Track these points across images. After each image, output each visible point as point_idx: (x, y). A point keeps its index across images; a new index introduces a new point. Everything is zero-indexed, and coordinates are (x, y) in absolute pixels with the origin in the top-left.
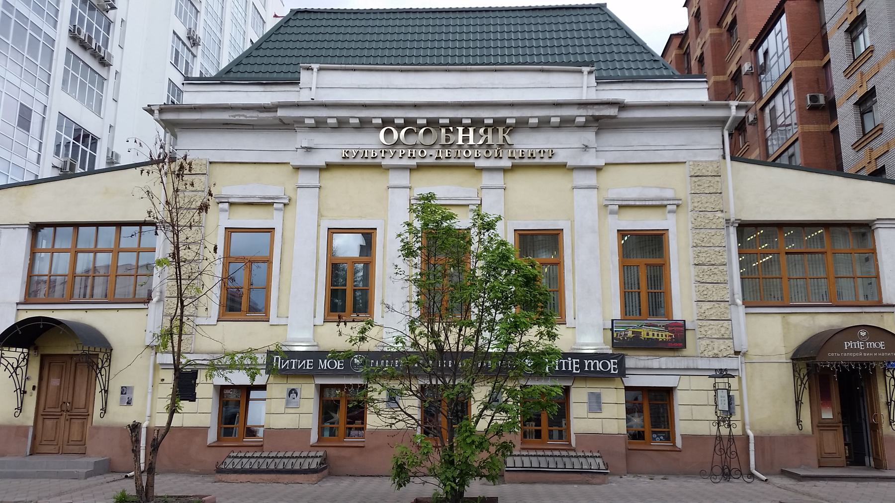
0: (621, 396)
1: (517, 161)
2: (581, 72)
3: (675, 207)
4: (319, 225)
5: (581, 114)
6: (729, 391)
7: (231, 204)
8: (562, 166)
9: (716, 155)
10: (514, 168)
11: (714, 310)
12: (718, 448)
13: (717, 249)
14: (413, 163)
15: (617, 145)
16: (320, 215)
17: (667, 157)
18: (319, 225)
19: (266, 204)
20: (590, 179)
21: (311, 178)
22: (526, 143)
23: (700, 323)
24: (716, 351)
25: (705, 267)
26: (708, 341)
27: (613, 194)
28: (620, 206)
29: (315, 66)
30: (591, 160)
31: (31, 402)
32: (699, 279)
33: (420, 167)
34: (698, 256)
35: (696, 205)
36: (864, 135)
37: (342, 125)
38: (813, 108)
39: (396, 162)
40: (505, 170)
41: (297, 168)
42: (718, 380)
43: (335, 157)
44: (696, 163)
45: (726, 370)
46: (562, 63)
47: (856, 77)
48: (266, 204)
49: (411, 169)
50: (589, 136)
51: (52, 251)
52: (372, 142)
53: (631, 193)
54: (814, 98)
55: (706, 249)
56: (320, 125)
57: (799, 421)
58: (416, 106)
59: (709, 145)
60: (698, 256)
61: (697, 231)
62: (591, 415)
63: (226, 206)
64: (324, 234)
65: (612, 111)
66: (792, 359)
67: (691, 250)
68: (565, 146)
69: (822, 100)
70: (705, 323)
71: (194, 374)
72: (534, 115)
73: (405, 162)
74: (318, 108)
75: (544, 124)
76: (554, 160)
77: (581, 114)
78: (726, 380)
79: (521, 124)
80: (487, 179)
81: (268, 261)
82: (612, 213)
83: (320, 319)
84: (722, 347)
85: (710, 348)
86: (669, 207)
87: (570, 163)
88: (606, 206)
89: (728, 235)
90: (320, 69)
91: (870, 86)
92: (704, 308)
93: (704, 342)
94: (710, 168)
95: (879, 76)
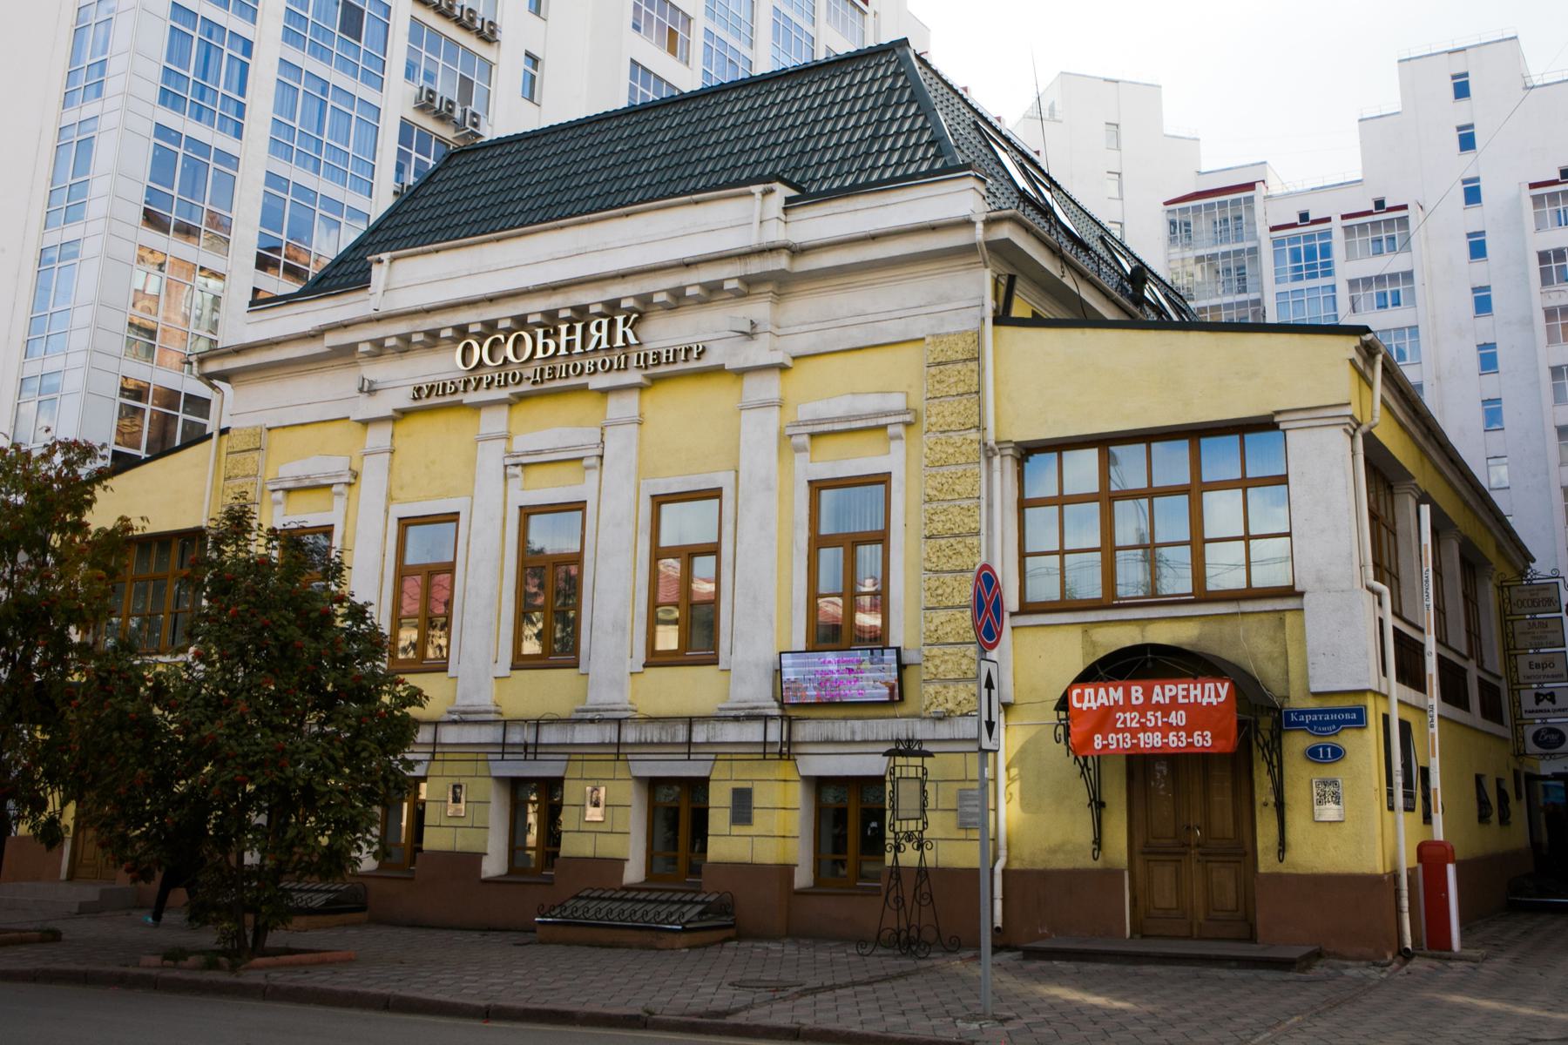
0: (796, 795)
2: (752, 194)
3: (806, 439)
4: (387, 511)
6: (923, 783)
7: (288, 491)
8: (719, 370)
10: (655, 380)
11: (953, 625)
12: (893, 894)
13: (965, 504)
15: (808, 318)
16: (390, 498)
17: (893, 331)
18: (387, 511)
20: (769, 387)
21: (379, 437)
22: (663, 333)
23: (926, 650)
24: (950, 706)
25: (943, 542)
26: (939, 687)
27: (806, 411)
28: (812, 435)
29: (385, 256)
30: (758, 353)
32: (929, 565)
33: (522, 397)
34: (931, 520)
35: (933, 420)
37: (406, 345)
40: (640, 387)
41: (365, 423)
42: (900, 760)
43: (403, 400)
45: (920, 742)
46: (717, 187)
49: (640, 387)
50: (758, 309)
51: (1107, 498)
52: (446, 365)
55: (945, 505)
56: (379, 349)
58: (491, 300)
60: (931, 520)
61: (934, 471)
62: (737, 830)
63: (280, 495)
64: (514, 515)
65: (781, 262)
70: (935, 650)
74: (295, 344)
75: (678, 299)
76: (709, 361)
77: (727, 273)
78: (917, 761)
79: (642, 311)
81: (881, 538)
84: (962, 696)
85: (941, 699)
86: (891, 430)
89: (344, 538)
90: (393, 259)
92: (936, 622)
93: (931, 689)
94: (961, 344)
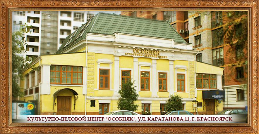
1: (160, 58)
5: (173, 50)
8: (168, 60)
9: (194, 60)
14: (140, 57)
19: (108, 64)
21: (118, 58)
22: (161, 54)
27: (176, 66)
31: (56, 107)
33: (141, 58)
36: (196, 45)
38: (181, 33)
39: (136, 56)
44: (190, 61)
47: (196, 30)
48: (108, 64)
53: (180, 66)
54: (182, 31)
57: (204, 109)
59: (193, 58)
66: (173, 98)
67: (189, 78)
68: (169, 56)
69: (183, 32)
71: (95, 101)
72: (165, 50)
73: (138, 56)
80: (153, 61)
82: (176, 70)
83: (158, 91)
86: (186, 70)
87: (170, 59)
88: (175, 69)
91: (200, 34)
95: (202, 32)
